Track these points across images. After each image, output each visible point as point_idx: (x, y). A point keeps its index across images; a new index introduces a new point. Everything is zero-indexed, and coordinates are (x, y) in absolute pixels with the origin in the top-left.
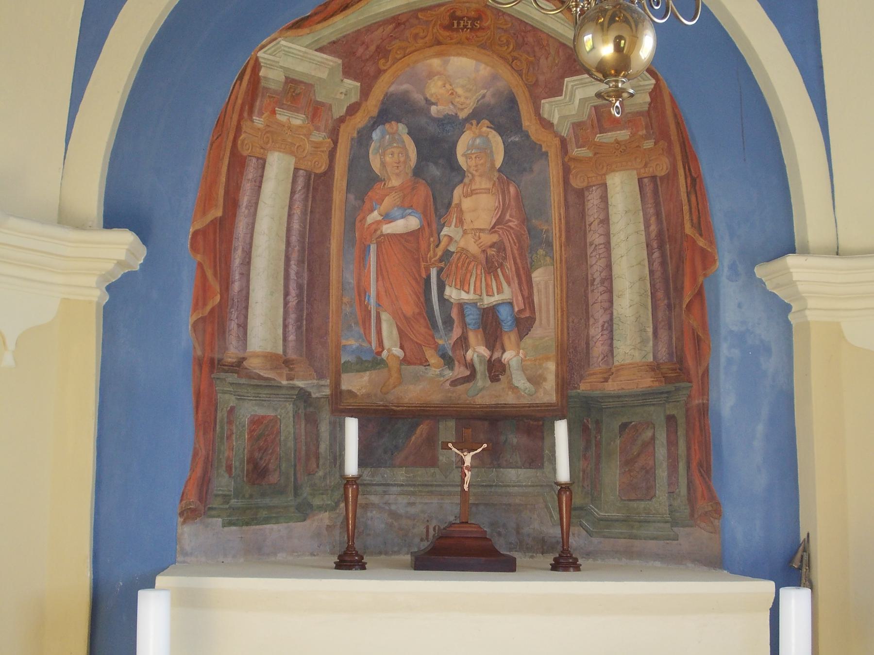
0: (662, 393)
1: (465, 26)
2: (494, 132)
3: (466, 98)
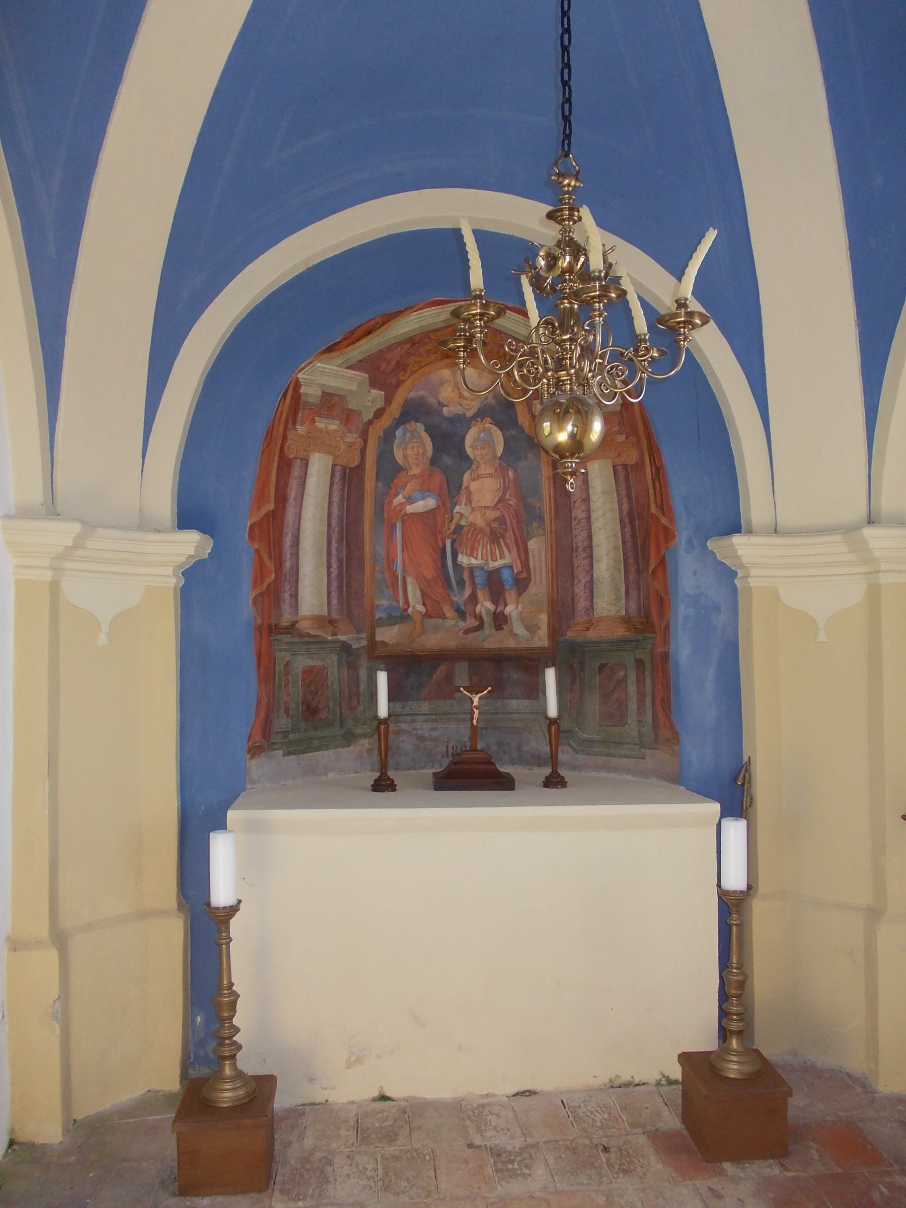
2: (495, 427)
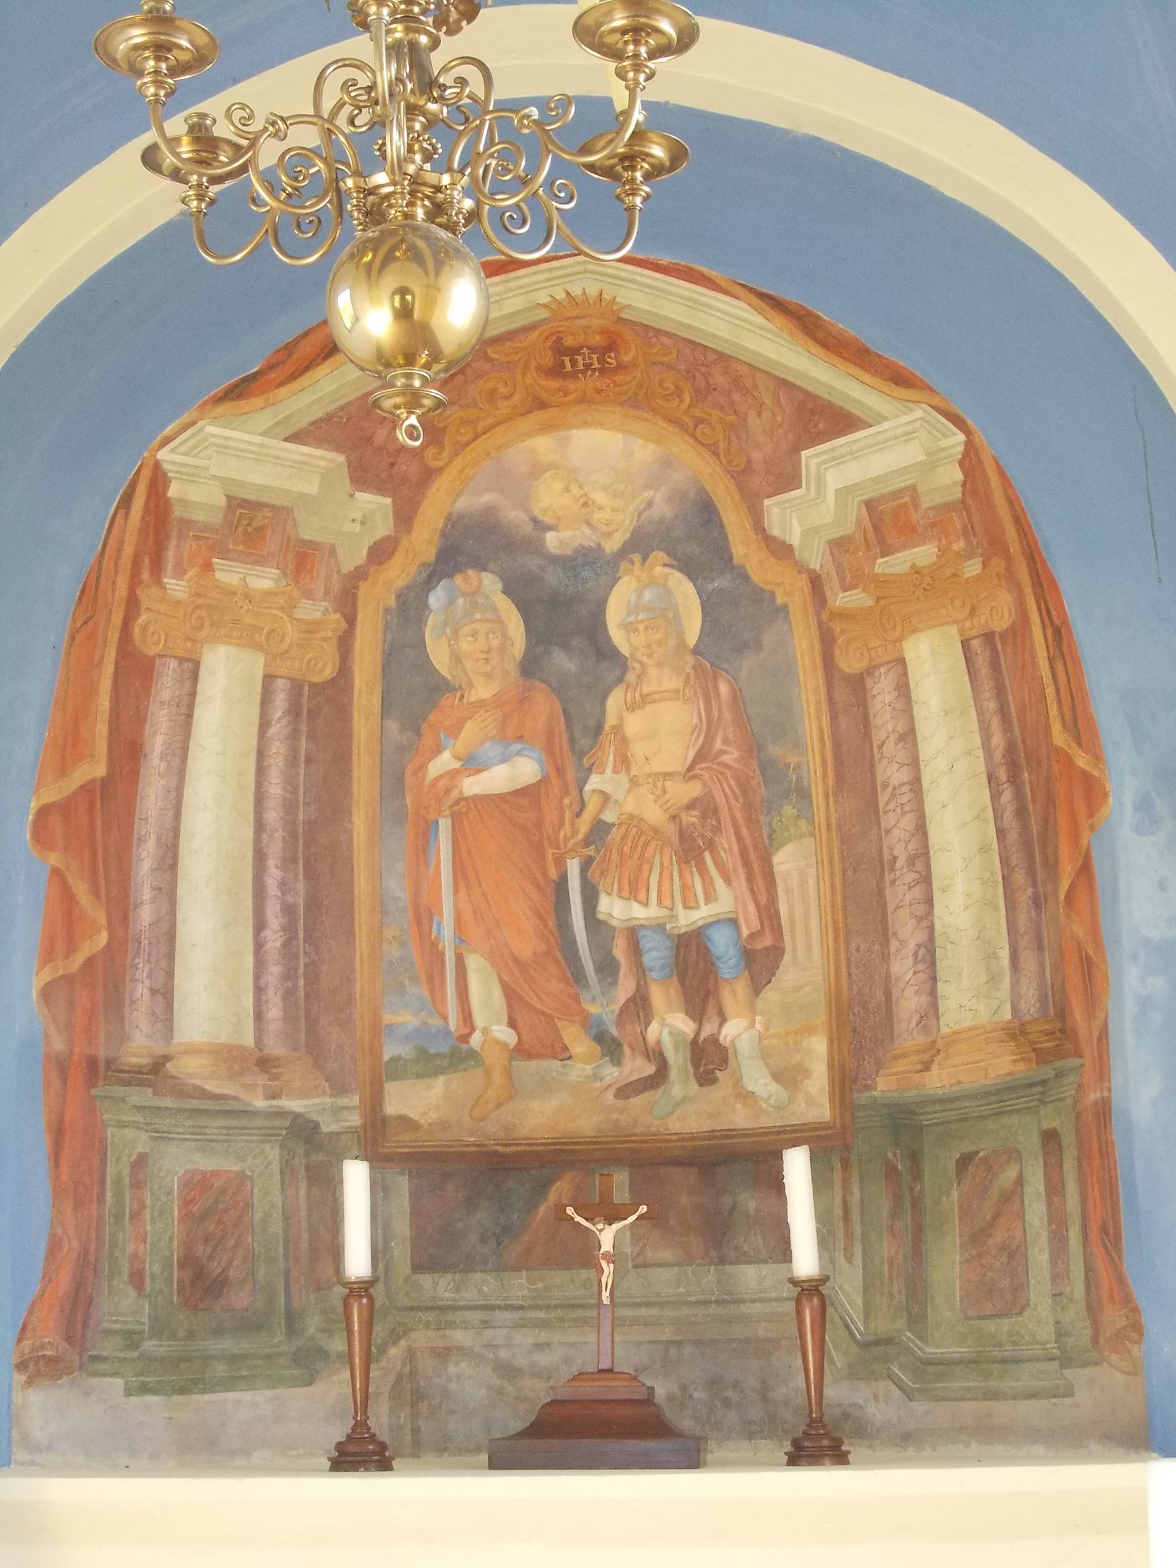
0: (1032, 1085)
1: (588, 367)
2: (678, 575)
3: (615, 510)
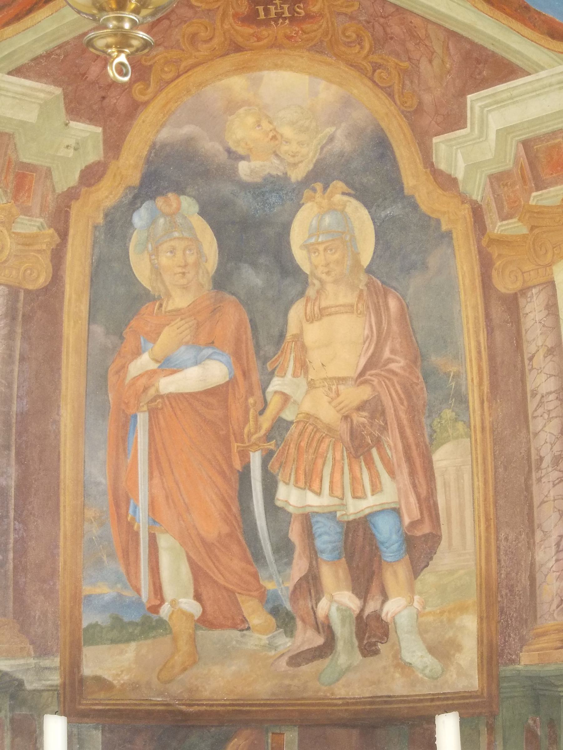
1: (279, 15)
